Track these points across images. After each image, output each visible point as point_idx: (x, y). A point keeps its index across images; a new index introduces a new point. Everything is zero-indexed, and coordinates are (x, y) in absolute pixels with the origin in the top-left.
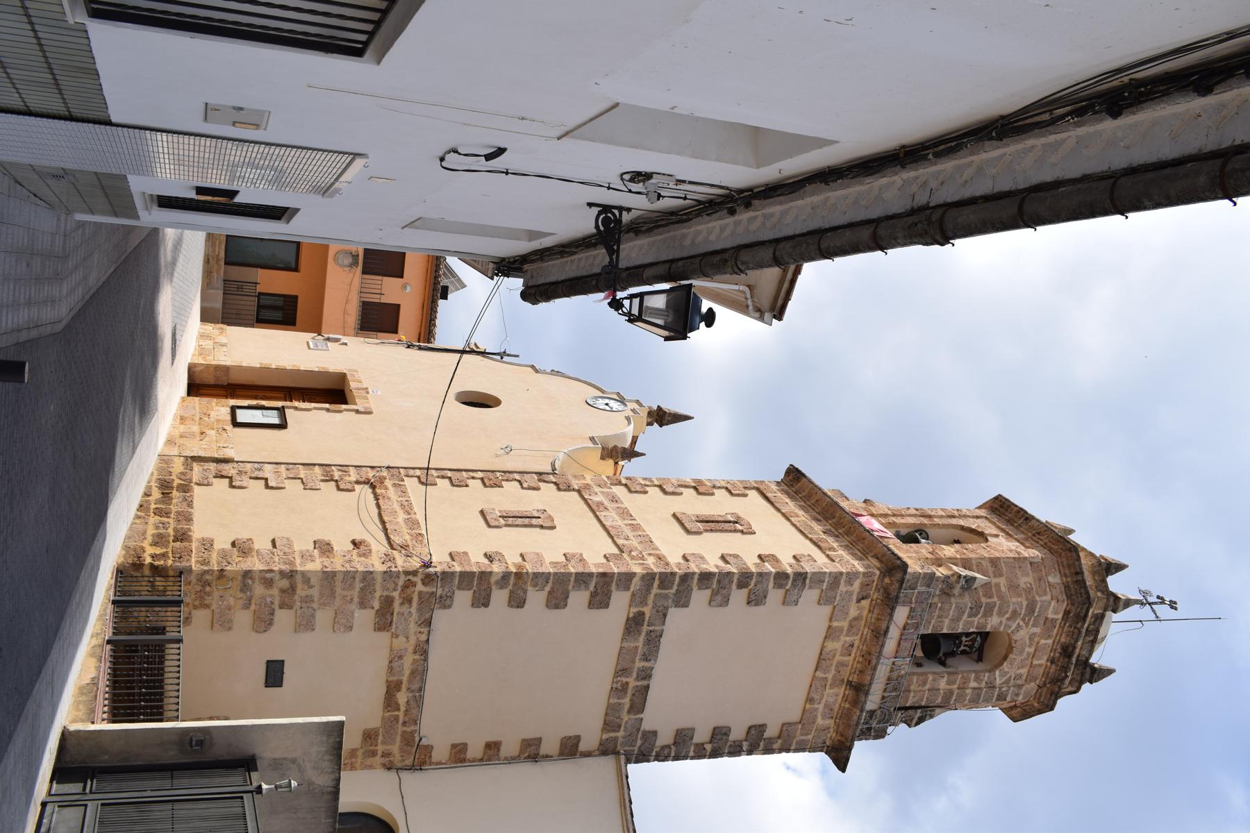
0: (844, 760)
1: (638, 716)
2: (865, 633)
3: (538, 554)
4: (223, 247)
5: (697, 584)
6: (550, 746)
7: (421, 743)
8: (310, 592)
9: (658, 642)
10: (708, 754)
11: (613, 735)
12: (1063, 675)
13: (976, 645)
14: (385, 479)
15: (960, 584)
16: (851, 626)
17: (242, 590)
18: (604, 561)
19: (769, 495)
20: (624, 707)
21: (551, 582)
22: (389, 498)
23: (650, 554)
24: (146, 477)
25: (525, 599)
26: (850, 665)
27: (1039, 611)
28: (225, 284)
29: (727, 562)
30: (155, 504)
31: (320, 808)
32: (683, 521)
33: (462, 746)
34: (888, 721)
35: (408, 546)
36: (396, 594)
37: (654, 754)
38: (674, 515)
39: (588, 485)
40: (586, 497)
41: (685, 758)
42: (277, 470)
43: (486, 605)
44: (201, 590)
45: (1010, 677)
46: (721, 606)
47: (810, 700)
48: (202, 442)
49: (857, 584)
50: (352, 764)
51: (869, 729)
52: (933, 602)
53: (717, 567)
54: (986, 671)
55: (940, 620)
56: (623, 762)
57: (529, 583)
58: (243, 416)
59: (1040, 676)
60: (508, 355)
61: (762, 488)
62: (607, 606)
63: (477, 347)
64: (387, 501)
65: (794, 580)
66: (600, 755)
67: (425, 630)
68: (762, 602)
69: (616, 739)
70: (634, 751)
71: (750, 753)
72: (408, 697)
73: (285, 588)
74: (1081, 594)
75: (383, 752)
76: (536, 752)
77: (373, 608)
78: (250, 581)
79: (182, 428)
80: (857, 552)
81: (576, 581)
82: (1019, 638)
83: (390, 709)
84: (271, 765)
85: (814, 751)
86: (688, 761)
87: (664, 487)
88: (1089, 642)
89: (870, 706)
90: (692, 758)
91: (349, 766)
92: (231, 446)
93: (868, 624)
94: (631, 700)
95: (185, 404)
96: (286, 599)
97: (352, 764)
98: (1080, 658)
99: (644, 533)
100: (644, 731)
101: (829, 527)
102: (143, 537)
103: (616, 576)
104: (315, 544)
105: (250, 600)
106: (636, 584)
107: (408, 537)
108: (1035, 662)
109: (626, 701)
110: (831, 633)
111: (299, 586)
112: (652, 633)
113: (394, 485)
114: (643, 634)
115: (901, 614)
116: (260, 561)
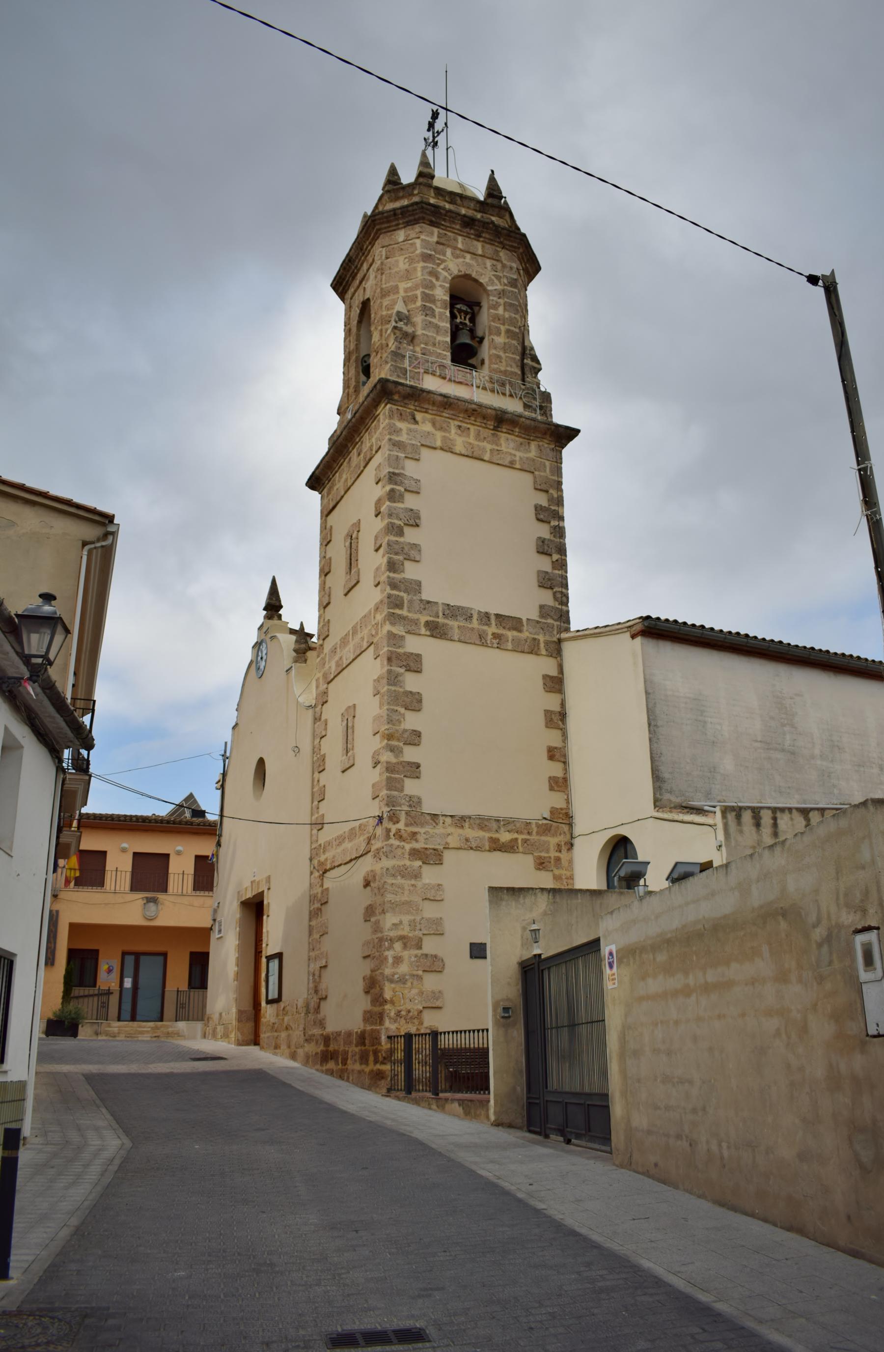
0: (568, 431)
1: (525, 623)
4: (144, 1024)
5: (399, 574)
6: (552, 702)
7: (549, 818)
9: (454, 608)
11: (542, 645)
12: (491, 226)
13: (465, 309)
14: (319, 861)
16: (441, 429)
17: (404, 983)
18: (379, 659)
21: (396, 708)
22: (334, 857)
23: (374, 618)
24: (318, 1074)
27: (430, 250)
29: (380, 546)
30: (339, 1065)
31: (567, 904)
32: (350, 586)
33: (551, 781)
34: (534, 391)
35: (368, 837)
36: (408, 847)
38: (346, 595)
39: (323, 676)
40: (332, 677)
43: (418, 766)
45: (493, 275)
46: (420, 551)
47: (511, 466)
48: (293, 1028)
49: (400, 425)
50: (567, 878)
51: (541, 408)
52: (420, 352)
53: (383, 556)
54: (488, 299)
55: (437, 344)
57: (397, 728)
58: (273, 994)
59: (494, 247)
60: (225, 752)
61: (326, 513)
62: (419, 656)
63: (219, 781)
65: (396, 484)
67: (441, 819)
68: (416, 513)
69: (547, 643)
71: (561, 518)
72: (505, 832)
73: (402, 945)
75: (557, 851)
77: (420, 866)
78: (396, 976)
79: (284, 1047)
80: (373, 424)
81: (395, 685)
82: (457, 268)
84: (528, 948)
85: (561, 459)
86: (569, 575)
87: (325, 604)
88: (462, 201)
91: (570, 881)
92: (295, 1001)
93: (439, 413)
94: (509, 629)
96: (413, 943)
97: (567, 878)
98: (478, 209)
99: (359, 623)
101: (355, 450)
103: (390, 649)
104: (368, 921)
105: (414, 975)
106: (398, 630)
107: (362, 838)
108: (480, 252)
109: (510, 634)
111: (400, 933)
112: (446, 613)
113: (324, 852)
114: (446, 621)
115: (431, 383)
116: (379, 969)
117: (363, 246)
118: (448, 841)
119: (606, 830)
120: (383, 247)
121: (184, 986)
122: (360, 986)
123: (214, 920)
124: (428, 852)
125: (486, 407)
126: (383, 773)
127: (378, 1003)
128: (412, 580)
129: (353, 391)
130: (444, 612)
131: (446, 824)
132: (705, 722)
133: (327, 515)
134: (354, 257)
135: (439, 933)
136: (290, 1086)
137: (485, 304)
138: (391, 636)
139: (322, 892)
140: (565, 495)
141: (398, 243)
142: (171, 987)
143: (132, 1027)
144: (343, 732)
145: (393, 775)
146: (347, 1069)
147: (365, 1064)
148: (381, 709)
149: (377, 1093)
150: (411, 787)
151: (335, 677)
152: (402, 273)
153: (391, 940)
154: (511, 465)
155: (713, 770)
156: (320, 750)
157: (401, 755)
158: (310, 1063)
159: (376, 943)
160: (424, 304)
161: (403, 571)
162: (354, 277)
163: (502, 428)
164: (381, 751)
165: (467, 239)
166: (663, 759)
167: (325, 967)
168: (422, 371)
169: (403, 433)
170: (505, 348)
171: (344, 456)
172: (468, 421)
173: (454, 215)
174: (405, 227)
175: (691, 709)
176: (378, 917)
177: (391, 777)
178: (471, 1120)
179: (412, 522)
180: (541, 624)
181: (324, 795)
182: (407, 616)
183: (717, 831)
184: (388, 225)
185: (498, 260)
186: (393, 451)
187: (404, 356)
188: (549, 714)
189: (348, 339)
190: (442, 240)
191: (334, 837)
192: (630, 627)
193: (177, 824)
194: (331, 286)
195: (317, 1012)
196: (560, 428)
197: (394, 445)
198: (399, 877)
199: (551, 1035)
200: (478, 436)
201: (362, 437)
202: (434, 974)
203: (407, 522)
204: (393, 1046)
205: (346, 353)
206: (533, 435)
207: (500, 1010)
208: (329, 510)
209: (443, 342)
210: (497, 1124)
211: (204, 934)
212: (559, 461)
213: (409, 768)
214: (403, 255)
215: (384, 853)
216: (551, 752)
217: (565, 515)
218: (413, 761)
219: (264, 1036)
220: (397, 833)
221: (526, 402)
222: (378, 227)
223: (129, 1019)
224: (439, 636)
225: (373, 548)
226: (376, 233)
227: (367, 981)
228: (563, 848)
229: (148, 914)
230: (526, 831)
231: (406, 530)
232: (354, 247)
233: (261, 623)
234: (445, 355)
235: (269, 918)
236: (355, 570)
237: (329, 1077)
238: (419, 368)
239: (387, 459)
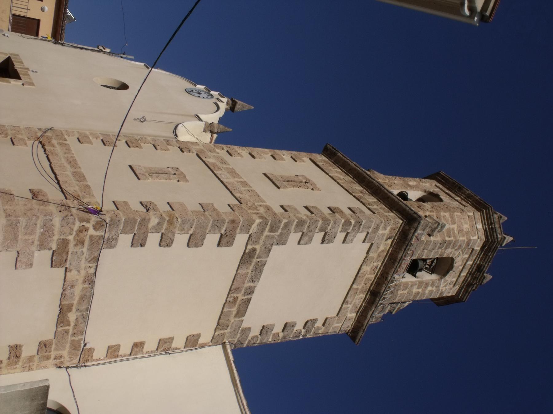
1: (241, 319)
5: (295, 228)
9: (262, 269)
16: (379, 256)
19: (318, 163)
21: (194, 227)
22: (57, 155)
25: (173, 240)
26: (372, 281)
32: (274, 180)
33: (117, 347)
35: (79, 196)
36: (71, 238)
39: (202, 150)
43: (142, 246)
49: (389, 228)
65: (354, 226)
68: (332, 240)
72: (77, 316)
75: (56, 356)
76: (169, 347)
81: (213, 226)
82: (457, 261)
83: (62, 325)
87: (253, 154)
97: (29, 366)
99: (252, 189)
103: (241, 222)
106: (254, 228)
109: (234, 310)
112: (259, 263)
113: (60, 144)
114: (253, 264)
118: (72, 272)
128: (288, 238)
131: (88, 269)
138: (251, 223)
141: (476, 224)
145: (137, 224)
150: (125, 239)
151: (204, 162)
152: (461, 227)
154: (345, 302)
160: (447, 242)
165: (470, 267)
169: (383, 231)
174: (483, 229)
179: (327, 237)
182: (263, 235)
191: (75, 155)
198: (42, 230)
200: (368, 279)
208: (315, 161)
214: (470, 227)
216: (140, 344)
224: (243, 259)
228: (59, 361)
230: (75, 331)
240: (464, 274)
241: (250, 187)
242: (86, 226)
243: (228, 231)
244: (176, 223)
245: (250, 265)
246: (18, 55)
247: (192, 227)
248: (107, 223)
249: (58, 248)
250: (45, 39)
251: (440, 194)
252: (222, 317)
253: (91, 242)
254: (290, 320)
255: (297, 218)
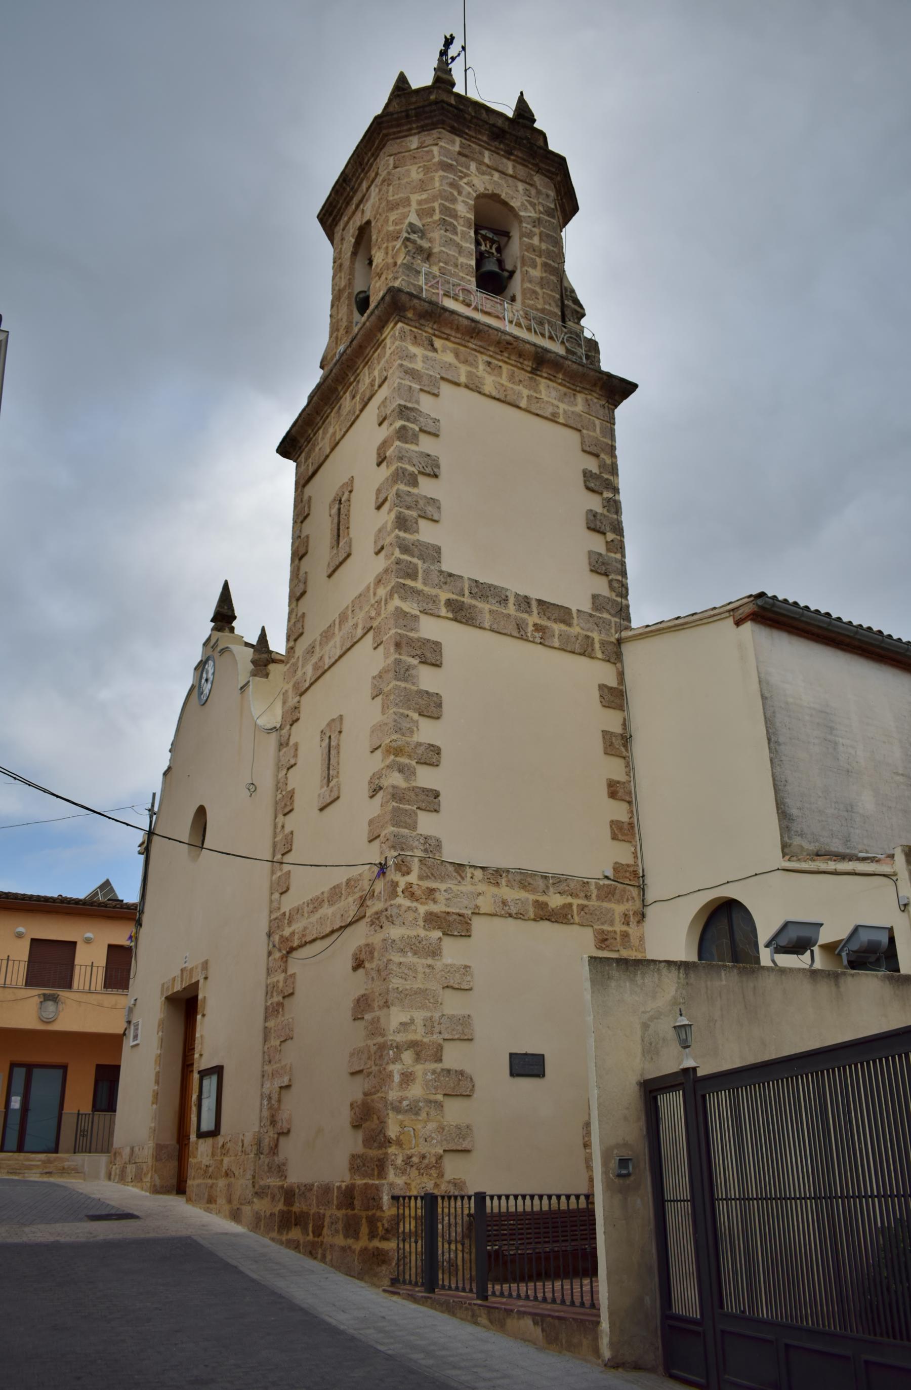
1: (575, 615)
2: (474, 347)
3: (373, 732)
4: (33, 1156)
6: (612, 721)
7: (612, 878)
8: (419, 1022)
9: (484, 586)
10: (619, 538)
13: (491, 236)
14: (282, 936)
15: (417, 239)
16: (466, 362)
18: (381, 648)
19: (310, 473)
20: (564, 631)
21: (406, 712)
22: (305, 928)
23: (375, 594)
24: (275, 1247)
25: (429, 744)
26: (513, 368)
27: (451, 159)
28: (79, 1152)
29: (386, 500)
30: (308, 1235)
31: (707, 988)
32: (337, 563)
35: (361, 897)
36: (422, 909)
37: (619, 599)
38: (330, 576)
39: (294, 686)
40: (307, 684)
41: (623, 564)
42: (271, 1075)
43: (437, 795)
44: (417, 1169)
45: (526, 200)
46: (439, 508)
47: (553, 419)
48: (237, 1174)
49: (414, 349)
55: (459, 267)
56: (630, 633)
57: (408, 739)
58: (207, 1124)
60: (153, 805)
61: (302, 482)
62: (438, 644)
63: (143, 843)
64: (308, 931)
65: (408, 420)
66: (622, 662)
67: (469, 871)
68: (434, 460)
69: (603, 643)
70: (616, 623)
71: (616, 490)
72: (555, 893)
74: (431, 112)
75: (623, 924)
76: (619, 738)
77: (440, 938)
78: (405, 1103)
80: (376, 354)
81: (405, 680)
82: (483, 186)
83: (570, 916)
84: (652, 1059)
87: (298, 594)
88: (488, 115)
89: (561, 351)
90: (623, 556)
92: (241, 1137)
93: (463, 342)
94: (555, 621)
95: (194, 1197)
99: (350, 605)
100: (593, 609)
101: (348, 394)
102: (348, 1250)
103: (399, 631)
104: (359, 1019)
105: (431, 1102)
106: (410, 607)
107: (350, 899)
108: (510, 172)
110: (474, 387)
111: (411, 1037)
112: (473, 592)
113: (290, 923)
114: (474, 602)
116: (378, 1091)
117: (363, 159)
119: (680, 898)
120: (390, 156)
121: (87, 1108)
122: (345, 1116)
123: (129, 1022)
124: (451, 918)
125: (524, 341)
126: (387, 802)
127: (375, 1144)
129: (344, 332)
130: (471, 590)
131: (476, 879)
132: (836, 743)
133: (304, 486)
134: (350, 176)
135: (466, 1038)
136: (235, 1270)
137: (515, 234)
138: (400, 614)
139: (286, 981)
140: (619, 463)
141: (410, 151)
142: (70, 1108)
143: (16, 1160)
144: (322, 755)
145: (401, 806)
146: (322, 1242)
147: (353, 1237)
148: (383, 714)
149: (374, 1285)
150: (426, 824)
151: (311, 684)
153: (397, 1047)
154: (553, 418)
155: (850, 808)
156: (286, 784)
157: (413, 778)
158: (262, 1227)
159: (372, 1052)
160: (443, 217)
161: (417, 531)
162: (348, 203)
163: (541, 371)
164: (384, 772)
165: (495, 155)
166: (788, 788)
167: (288, 1087)
168: (441, 292)
170: (542, 283)
171: (331, 405)
172: (500, 357)
173: (481, 123)
174: (419, 133)
175: (818, 724)
176: (377, 1013)
177: (399, 808)
178: (560, 1352)
179: (428, 470)
180: (595, 618)
181: (291, 845)
182: (422, 591)
183: (899, 883)
184: (399, 129)
185: (531, 185)
186: (404, 379)
187: (418, 272)
188: (609, 736)
189: (339, 275)
190: (466, 152)
192: (733, 610)
193: (88, 905)
194: (318, 217)
195: (274, 1153)
196: (614, 380)
197: (406, 372)
198: (409, 954)
199: (722, 1207)
200: (511, 378)
201: (358, 375)
202: (460, 1099)
203: (422, 470)
204: (401, 1211)
205: (335, 292)
206: (579, 384)
207: (614, 1164)
208: (307, 478)
209: (466, 264)
210: (615, 1364)
211: (115, 1042)
212: (612, 421)
213: (425, 797)
214: (416, 164)
215: (387, 917)
217: (620, 487)
218: (430, 787)
219: (192, 1183)
220: (407, 888)
221: (569, 348)
222: (384, 132)
223: (15, 1149)
224: (464, 621)
225: (373, 505)
226: (382, 140)
227: (357, 1109)
228: (632, 919)
229: (45, 1015)
230: (582, 894)
231: (421, 480)
232: (352, 161)
233: (207, 636)
234: (470, 280)
235: (206, 1018)
236: (344, 541)
237: (292, 1253)
238: (438, 288)
239: (397, 389)
240: (509, 167)
241: (347, 608)
242: (404, 887)
243: (414, 653)
244: (400, 743)
245: (477, 607)
246: (163, 985)
247: (408, 716)
248: (399, 855)
249: (439, 928)
250: (134, 938)
251: (358, 224)
252: (569, 649)
253: (430, 878)
254: (581, 523)
255: (392, 531)
